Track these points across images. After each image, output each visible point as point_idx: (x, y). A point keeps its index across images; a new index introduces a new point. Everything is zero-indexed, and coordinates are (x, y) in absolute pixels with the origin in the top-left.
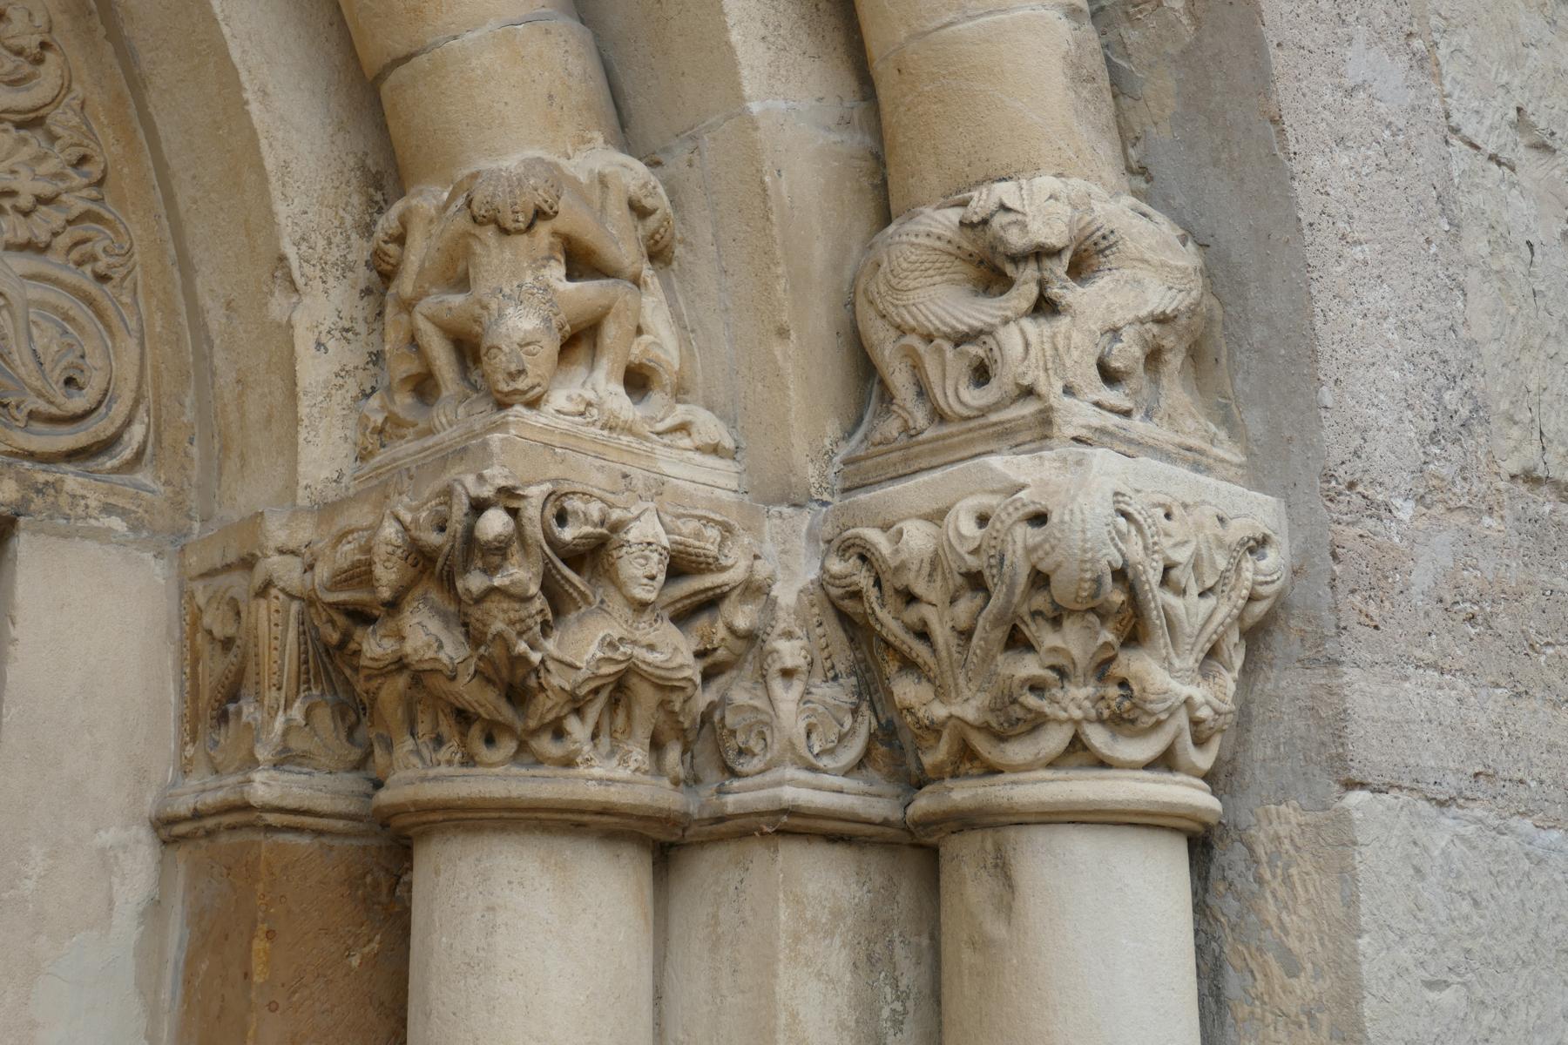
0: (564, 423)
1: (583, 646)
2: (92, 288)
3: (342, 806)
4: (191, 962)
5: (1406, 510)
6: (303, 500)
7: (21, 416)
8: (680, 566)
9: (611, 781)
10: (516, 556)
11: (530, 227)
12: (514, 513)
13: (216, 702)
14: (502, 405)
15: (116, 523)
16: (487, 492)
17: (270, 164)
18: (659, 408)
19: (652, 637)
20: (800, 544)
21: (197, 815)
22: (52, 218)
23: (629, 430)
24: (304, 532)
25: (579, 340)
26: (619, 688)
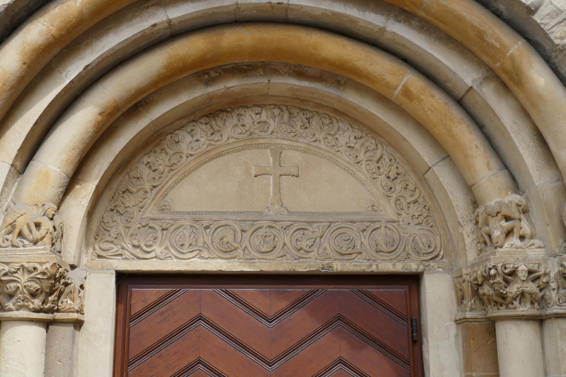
0: (507, 250)
1: (513, 289)
2: (430, 229)
3: (482, 317)
4: (463, 344)
6: (469, 265)
7: (422, 254)
8: (530, 272)
9: (524, 311)
10: (497, 277)
11: (497, 215)
12: (496, 269)
13: (461, 300)
14: (496, 248)
15: (440, 270)
16: (491, 267)
17: (454, 206)
18: (527, 242)
19: (527, 286)
20: (556, 264)
21: (460, 320)
23: (520, 248)
24: (469, 270)
25: (509, 233)
26: (522, 295)
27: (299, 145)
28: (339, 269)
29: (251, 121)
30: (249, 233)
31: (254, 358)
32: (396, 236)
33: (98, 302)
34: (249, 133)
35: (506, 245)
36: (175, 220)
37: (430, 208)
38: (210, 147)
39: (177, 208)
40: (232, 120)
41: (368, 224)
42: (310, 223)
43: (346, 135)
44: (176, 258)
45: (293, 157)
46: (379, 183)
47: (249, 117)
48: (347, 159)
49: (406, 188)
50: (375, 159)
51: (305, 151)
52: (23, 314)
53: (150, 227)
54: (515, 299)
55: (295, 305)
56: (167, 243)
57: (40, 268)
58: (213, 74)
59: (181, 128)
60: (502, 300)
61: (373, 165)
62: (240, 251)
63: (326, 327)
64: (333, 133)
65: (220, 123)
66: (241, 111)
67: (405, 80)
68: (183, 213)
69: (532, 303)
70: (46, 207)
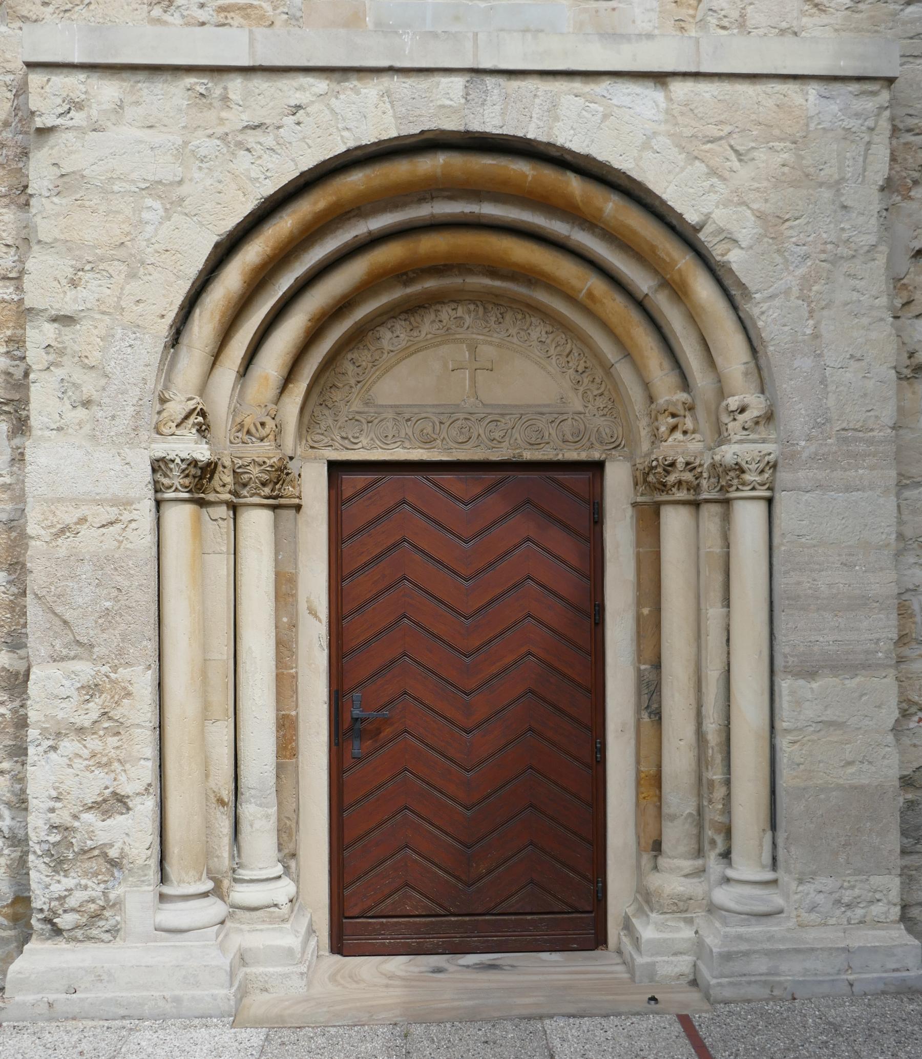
1: (672, 479)
5: (803, 443)
8: (687, 464)
13: (636, 484)
24: (642, 460)
25: (674, 428)
27: (493, 339)
29: (447, 317)
31: (451, 537)
32: (582, 427)
34: (445, 328)
35: (670, 439)
36: (379, 414)
37: (615, 400)
38: (410, 343)
39: (381, 402)
40: (430, 317)
41: (556, 416)
42: (503, 415)
43: (538, 331)
44: (382, 448)
45: (487, 351)
46: (567, 377)
47: (446, 313)
48: (538, 354)
49: (593, 382)
50: (565, 353)
51: (499, 346)
53: (357, 420)
54: (674, 487)
55: (489, 490)
56: (372, 435)
57: (269, 462)
58: (411, 275)
59: (382, 324)
60: (663, 487)
61: (563, 360)
63: (515, 510)
64: (525, 328)
65: (418, 319)
66: (439, 307)
67: (589, 284)
68: (386, 406)
69: (688, 490)
70: (269, 408)
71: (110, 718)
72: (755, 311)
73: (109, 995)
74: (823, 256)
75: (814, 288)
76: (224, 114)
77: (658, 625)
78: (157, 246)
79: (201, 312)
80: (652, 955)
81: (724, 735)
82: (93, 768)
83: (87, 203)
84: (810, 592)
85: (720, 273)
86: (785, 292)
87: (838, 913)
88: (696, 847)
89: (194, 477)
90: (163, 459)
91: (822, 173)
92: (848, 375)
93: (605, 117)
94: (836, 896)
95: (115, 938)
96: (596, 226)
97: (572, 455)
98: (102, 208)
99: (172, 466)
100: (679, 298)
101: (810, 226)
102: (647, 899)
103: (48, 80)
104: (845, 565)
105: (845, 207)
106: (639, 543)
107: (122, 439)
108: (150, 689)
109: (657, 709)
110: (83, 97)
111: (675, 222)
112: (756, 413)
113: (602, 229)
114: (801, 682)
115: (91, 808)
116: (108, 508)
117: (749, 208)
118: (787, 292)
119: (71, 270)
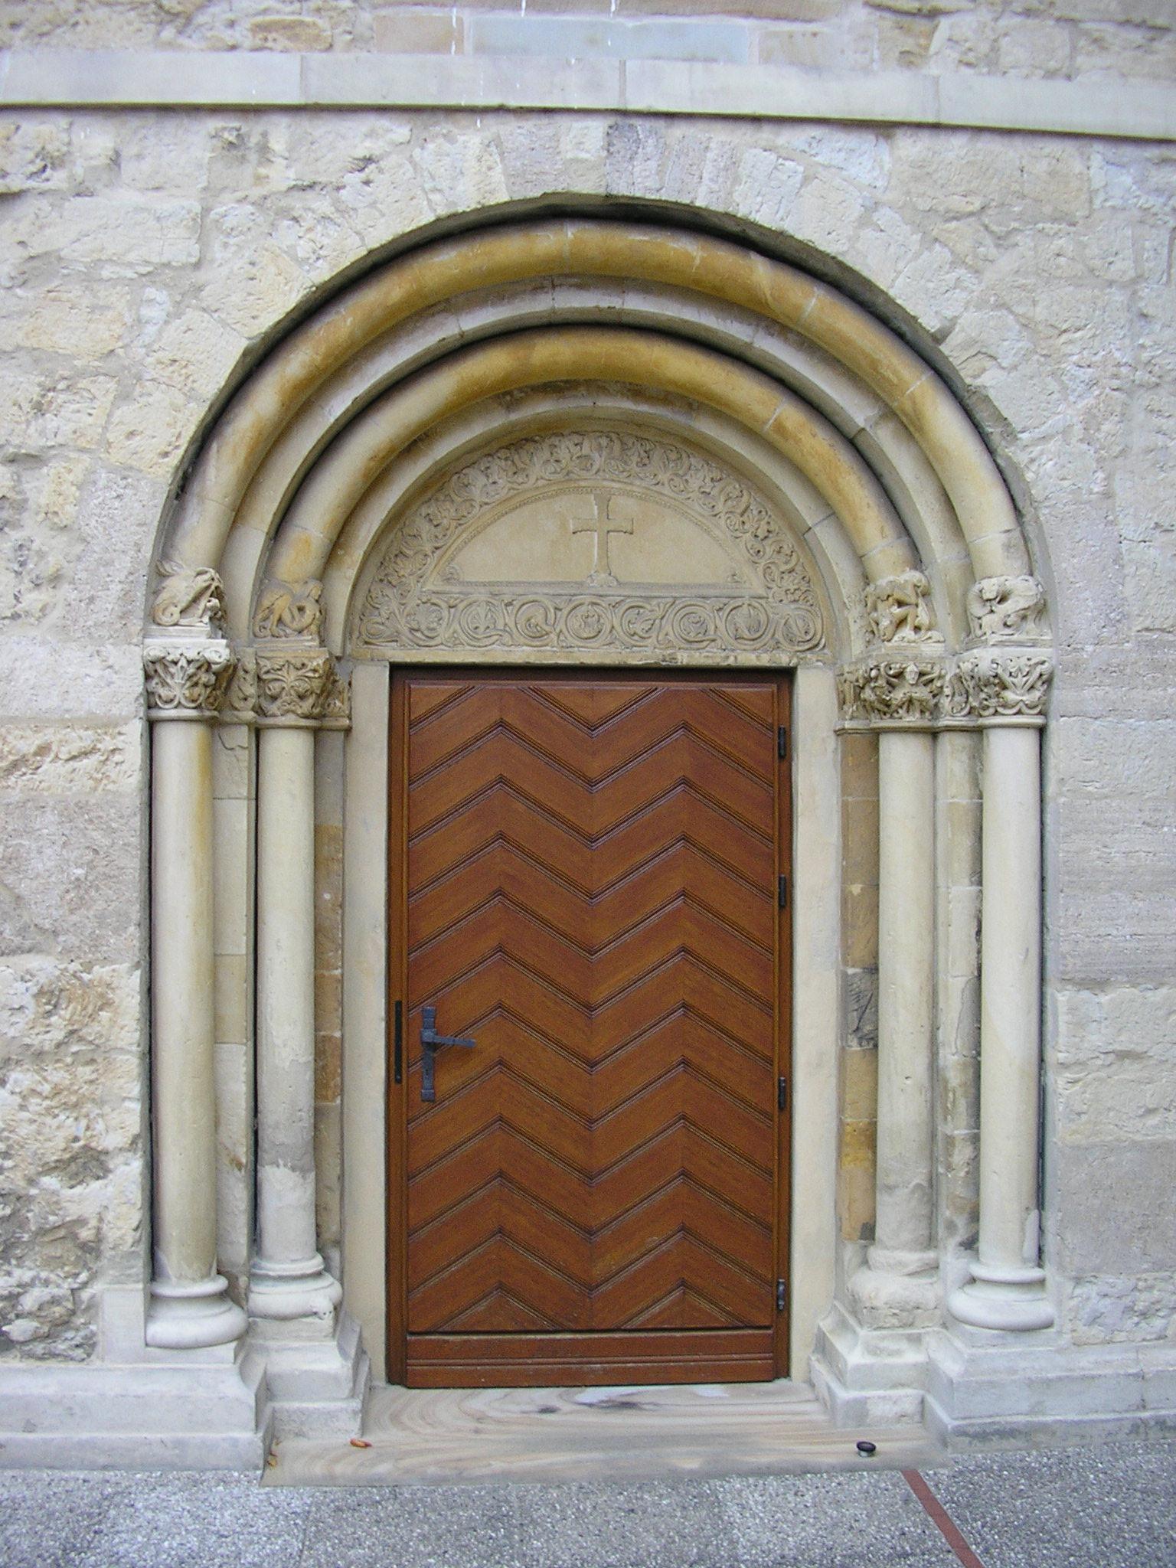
1: (898, 696)
5: (1090, 648)
13: (843, 703)
22: (798, 593)
24: (853, 668)
25: (901, 622)
28: (685, 662)
30: (565, 612)
32: (763, 618)
33: (370, 700)
35: (896, 638)
38: (512, 492)
41: (726, 601)
42: (647, 598)
43: (701, 476)
47: (566, 449)
50: (739, 511)
51: (643, 498)
52: (291, 720)
61: (736, 520)
62: (553, 636)
66: (555, 441)
68: (476, 584)
69: (922, 712)
71: (81, 1039)
72: (1022, 458)
73: (85, 1436)
74: (1115, 383)
75: (1105, 427)
76: (262, 171)
77: (874, 909)
78: (160, 355)
79: (219, 448)
80: (863, 1388)
81: (971, 1071)
82: (56, 1111)
83: (64, 296)
84: (1099, 863)
85: (970, 402)
86: (1064, 432)
87: (1129, 1323)
88: (926, 1232)
89: (206, 686)
90: (161, 660)
91: (1112, 268)
92: (1152, 551)
93: (806, 180)
94: (1127, 1301)
95: (89, 1355)
96: (791, 330)
97: (749, 658)
98: (85, 302)
99: (173, 669)
100: (910, 436)
101: (1097, 340)
102: (856, 1310)
103: (18, 128)
104: (1149, 825)
105: (1145, 316)
106: (845, 789)
107: (105, 633)
108: (138, 998)
109: (871, 1032)
110: (65, 149)
111: (904, 328)
112: (1023, 604)
113: (799, 334)
114: (1085, 994)
115: (56, 1168)
116: (82, 732)
117: (1012, 312)
118: (1066, 432)
119: (38, 389)
